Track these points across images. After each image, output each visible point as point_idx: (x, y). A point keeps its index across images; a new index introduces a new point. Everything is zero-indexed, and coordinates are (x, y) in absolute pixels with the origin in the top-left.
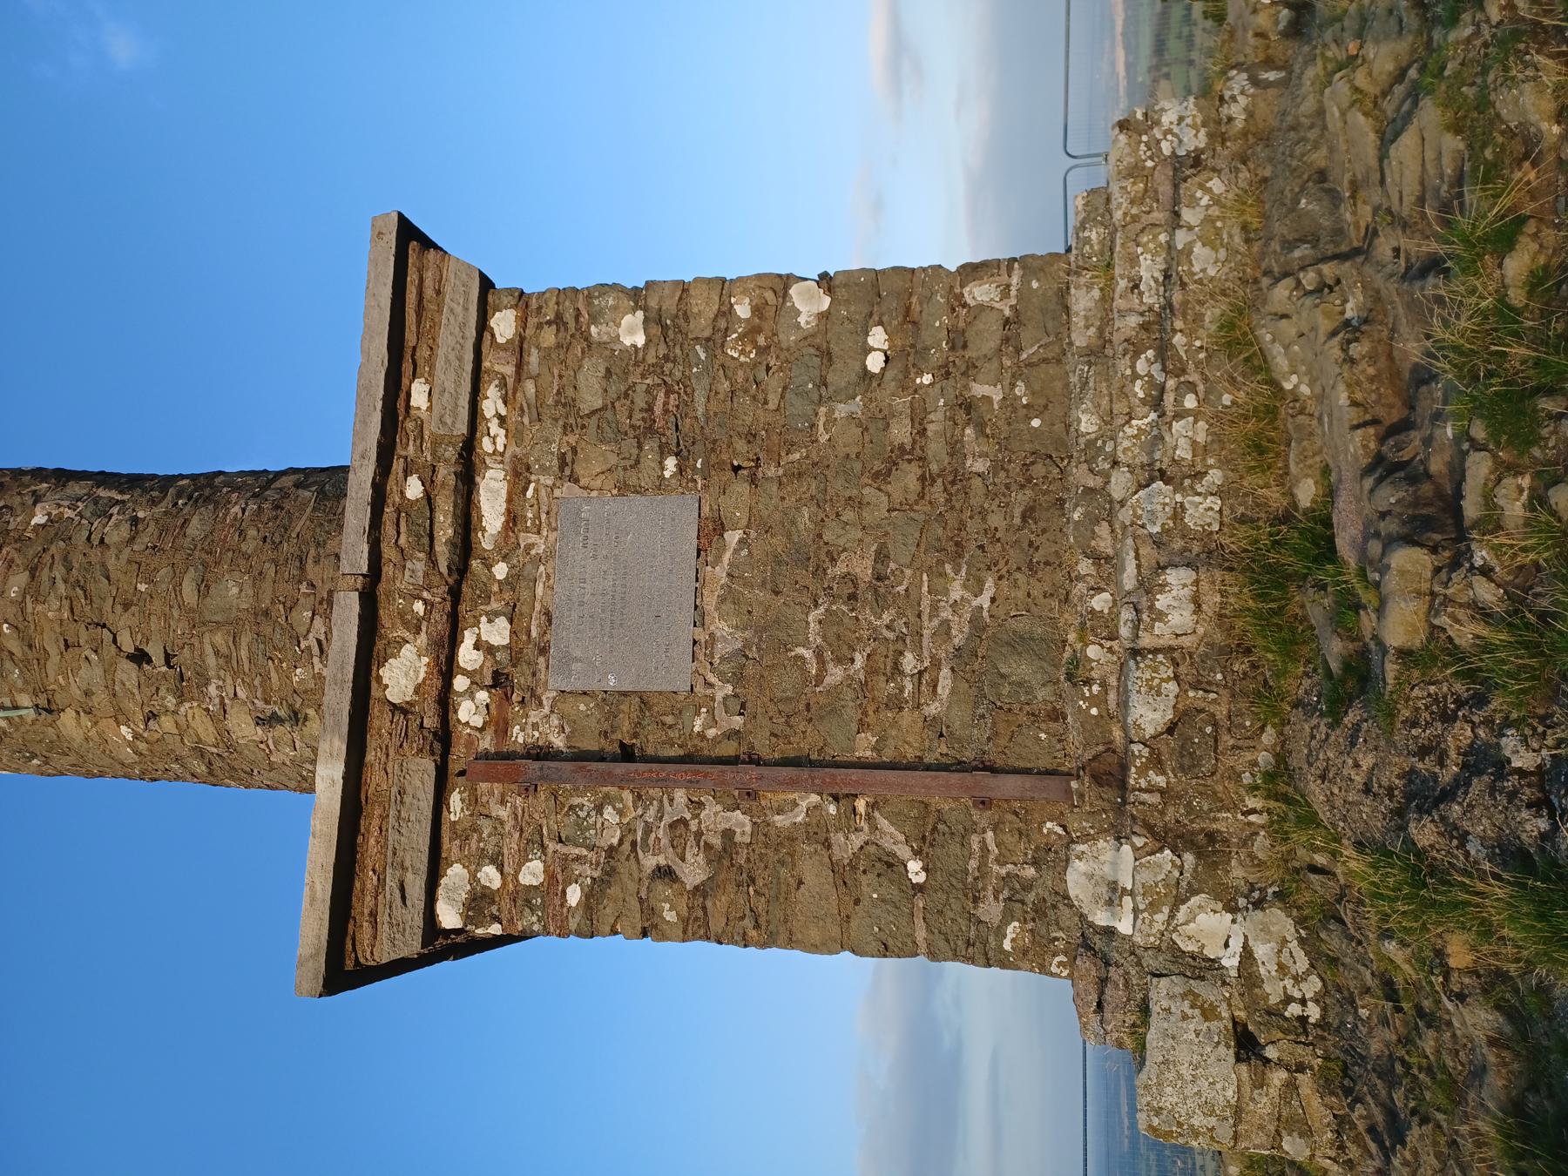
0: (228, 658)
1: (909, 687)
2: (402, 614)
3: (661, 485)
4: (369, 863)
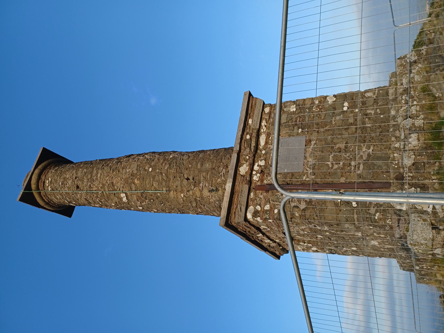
0: (205, 178)
1: (353, 168)
2: (244, 159)
3: (298, 134)
4: (235, 203)
